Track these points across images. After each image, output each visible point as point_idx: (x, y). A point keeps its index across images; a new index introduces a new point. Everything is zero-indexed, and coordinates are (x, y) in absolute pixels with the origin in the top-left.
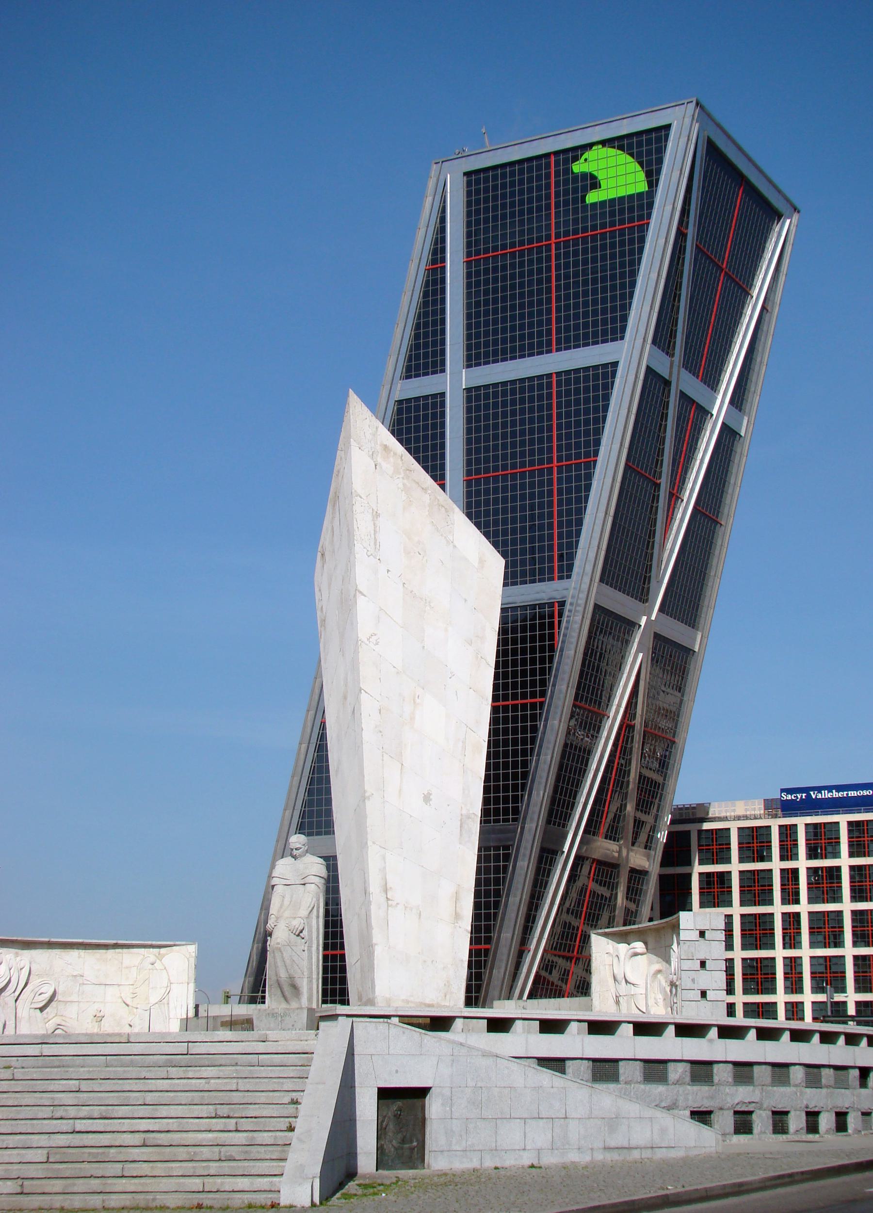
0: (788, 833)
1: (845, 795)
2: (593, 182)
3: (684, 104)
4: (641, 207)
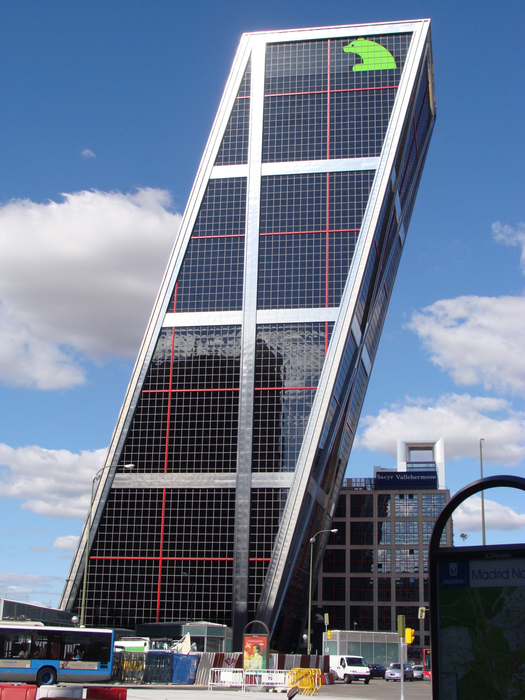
2: (359, 60)
3: (421, 21)
4: (391, 78)
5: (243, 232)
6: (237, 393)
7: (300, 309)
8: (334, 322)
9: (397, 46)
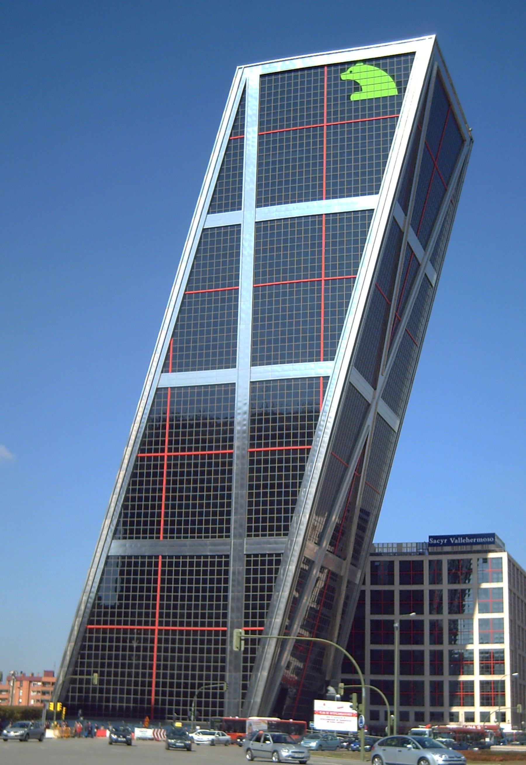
0: (435, 567)
1: (475, 541)
2: (357, 87)
4: (392, 106)
5: (237, 284)
6: (231, 455)
7: (198, 372)
8: (329, 377)
9: (399, 69)
